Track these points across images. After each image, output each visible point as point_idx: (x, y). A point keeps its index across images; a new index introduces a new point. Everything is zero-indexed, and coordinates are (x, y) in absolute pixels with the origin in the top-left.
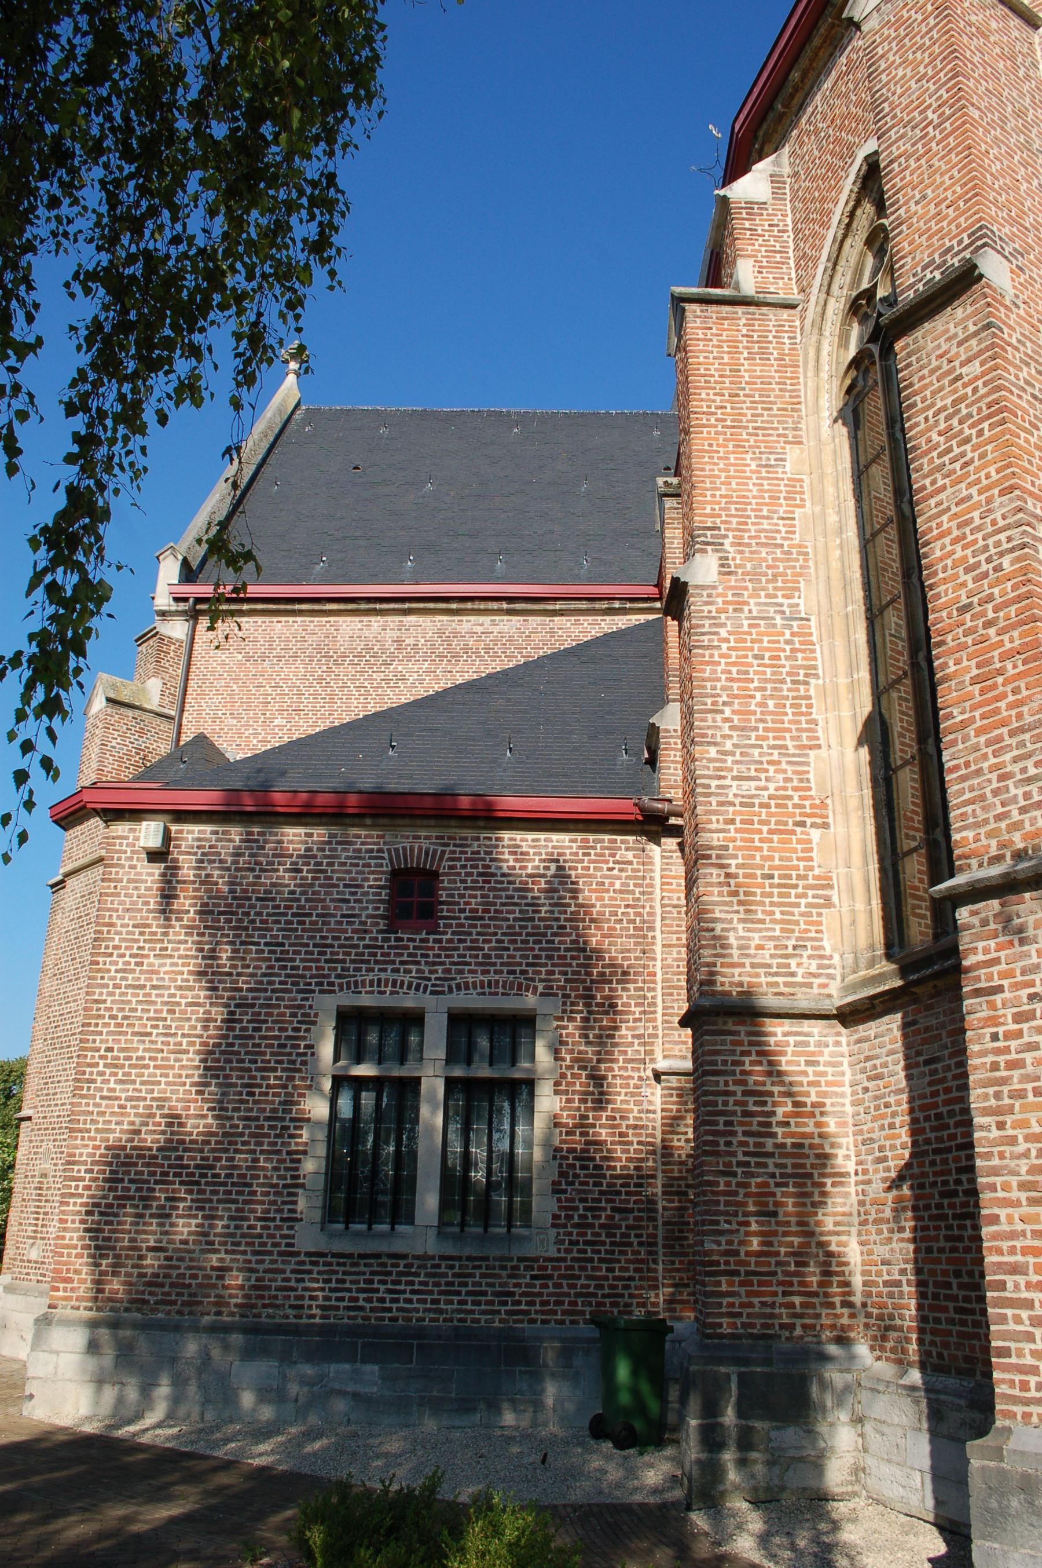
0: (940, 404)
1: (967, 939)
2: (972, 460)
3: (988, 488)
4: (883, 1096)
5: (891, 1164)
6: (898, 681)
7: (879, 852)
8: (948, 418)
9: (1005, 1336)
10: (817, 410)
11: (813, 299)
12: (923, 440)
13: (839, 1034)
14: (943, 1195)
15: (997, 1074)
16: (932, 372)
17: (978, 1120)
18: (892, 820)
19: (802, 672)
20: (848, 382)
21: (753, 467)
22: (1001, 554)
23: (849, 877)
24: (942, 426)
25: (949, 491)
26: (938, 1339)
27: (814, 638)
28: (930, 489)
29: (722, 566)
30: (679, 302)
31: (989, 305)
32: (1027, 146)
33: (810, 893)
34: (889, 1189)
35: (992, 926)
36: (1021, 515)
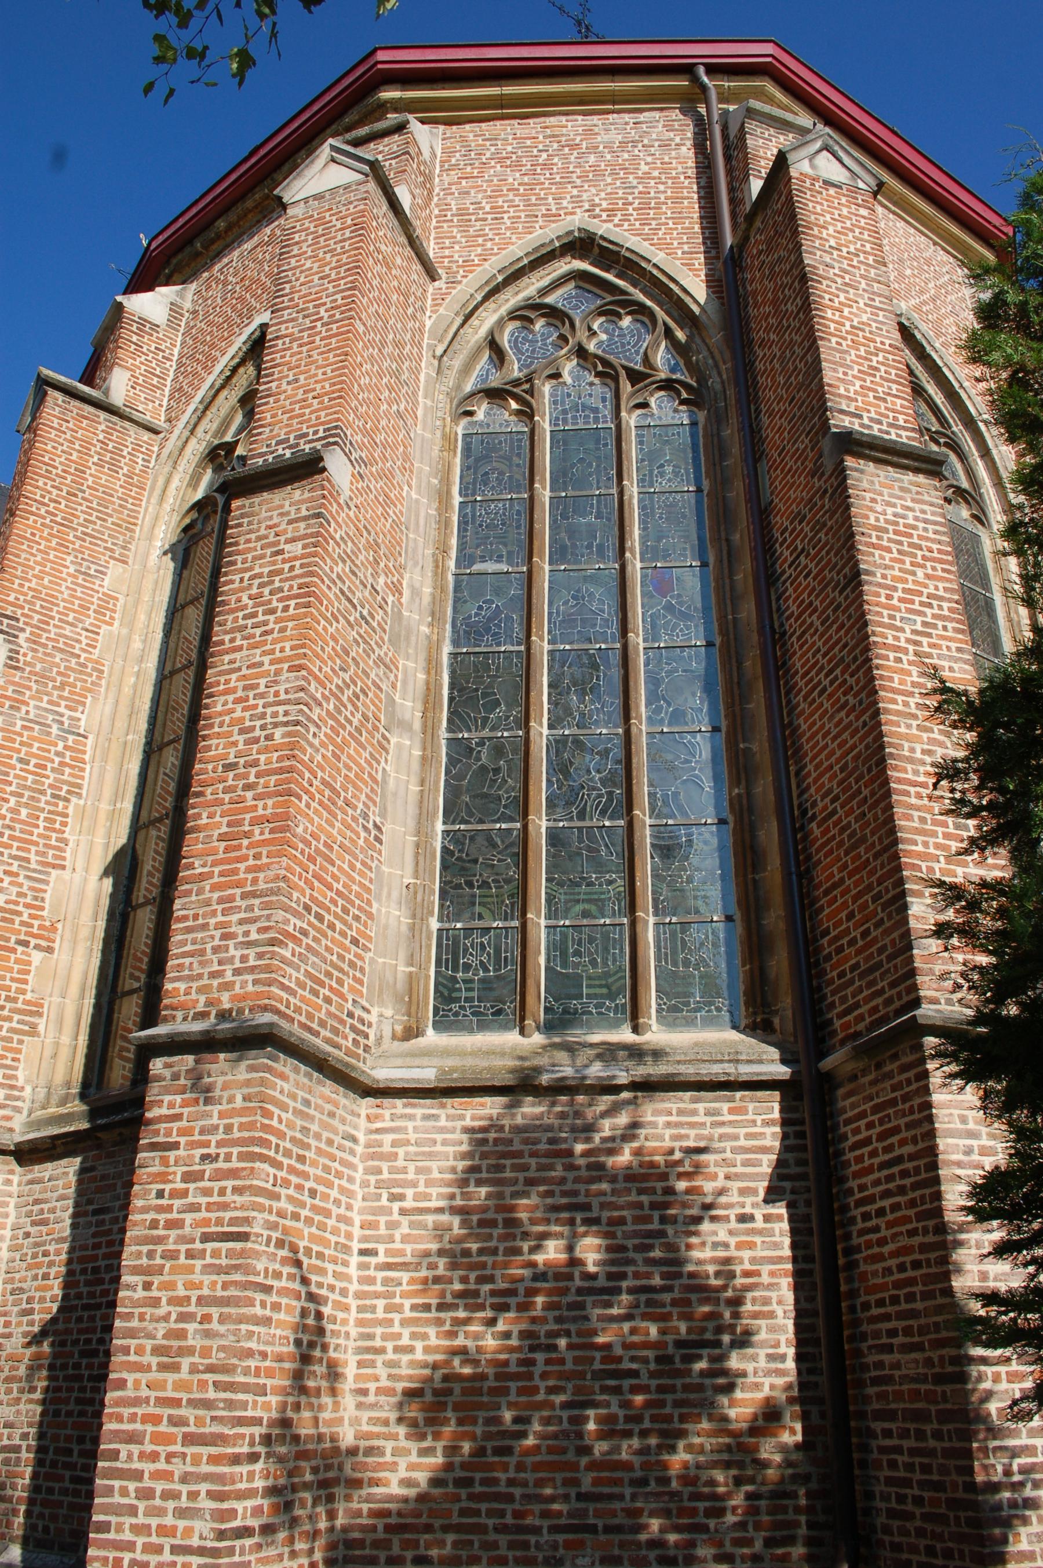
0: (257, 570)
1: (155, 1091)
2: (272, 631)
3: (280, 661)
4: (44, 1244)
5: (36, 1317)
6: (160, 820)
7: (98, 987)
8: (261, 586)
9: (108, 1509)
10: (151, 538)
11: (177, 432)
12: (233, 598)
13: (12, 1172)
14: (83, 1354)
15: (155, 1232)
16: (259, 539)
17: (126, 1279)
18: (119, 957)
19: (65, 788)
20: (187, 521)
21: (71, 570)
22: (276, 725)
23: (62, 1009)
24: (254, 591)
25: (245, 652)
26: (47, 1512)
27: (87, 757)
28: (227, 645)
29: (11, 658)
30: (43, 384)
31: (324, 497)
32: (396, 374)
33: (16, 1017)
34: (29, 1344)
35: (182, 1081)
36: (301, 694)
